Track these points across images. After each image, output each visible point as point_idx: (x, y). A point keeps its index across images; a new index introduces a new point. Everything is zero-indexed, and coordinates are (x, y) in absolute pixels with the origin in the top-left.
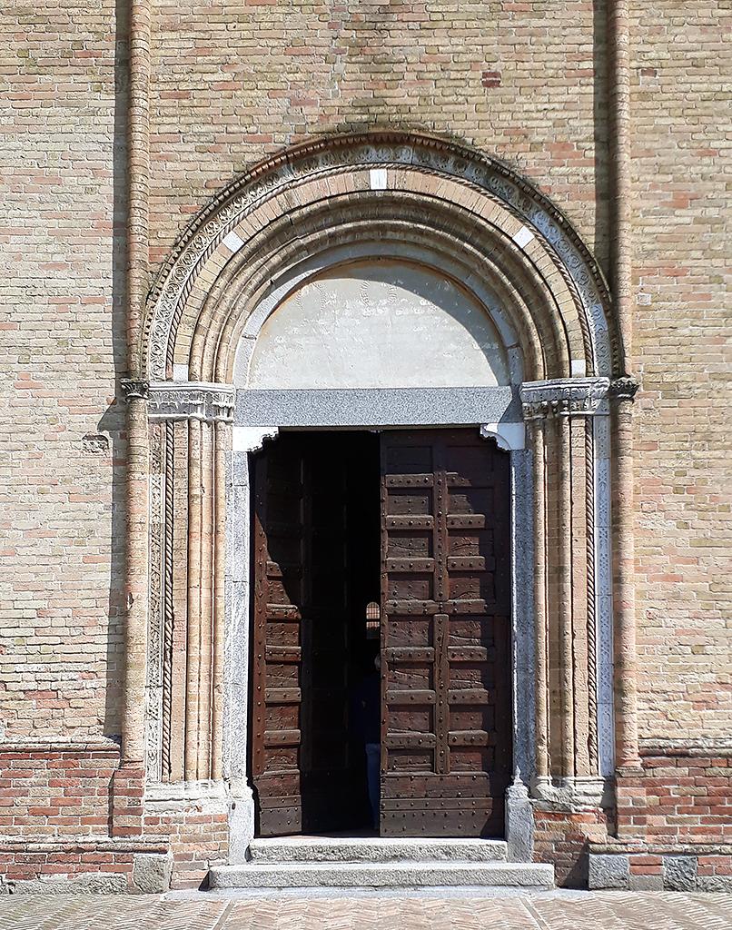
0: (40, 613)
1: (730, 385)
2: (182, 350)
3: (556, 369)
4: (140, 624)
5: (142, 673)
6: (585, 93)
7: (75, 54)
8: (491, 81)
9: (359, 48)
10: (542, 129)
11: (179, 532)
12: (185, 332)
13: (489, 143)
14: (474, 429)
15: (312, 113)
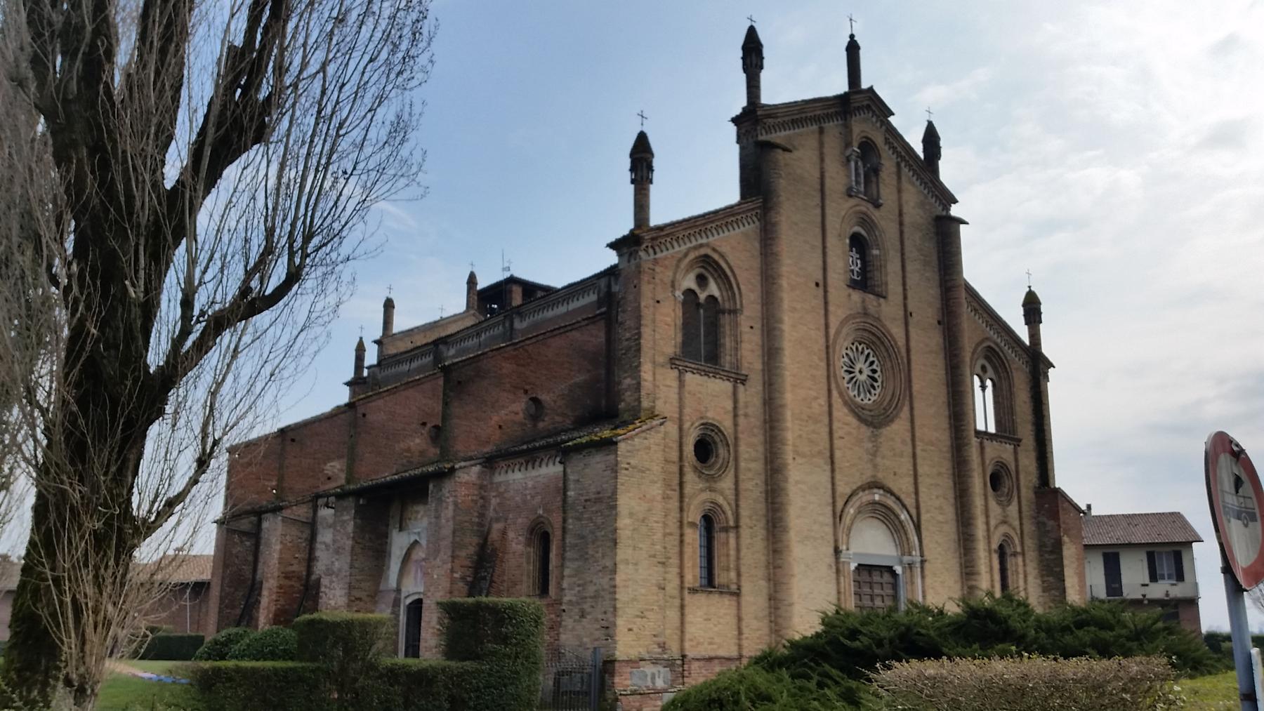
13: (895, 490)
14: (892, 567)
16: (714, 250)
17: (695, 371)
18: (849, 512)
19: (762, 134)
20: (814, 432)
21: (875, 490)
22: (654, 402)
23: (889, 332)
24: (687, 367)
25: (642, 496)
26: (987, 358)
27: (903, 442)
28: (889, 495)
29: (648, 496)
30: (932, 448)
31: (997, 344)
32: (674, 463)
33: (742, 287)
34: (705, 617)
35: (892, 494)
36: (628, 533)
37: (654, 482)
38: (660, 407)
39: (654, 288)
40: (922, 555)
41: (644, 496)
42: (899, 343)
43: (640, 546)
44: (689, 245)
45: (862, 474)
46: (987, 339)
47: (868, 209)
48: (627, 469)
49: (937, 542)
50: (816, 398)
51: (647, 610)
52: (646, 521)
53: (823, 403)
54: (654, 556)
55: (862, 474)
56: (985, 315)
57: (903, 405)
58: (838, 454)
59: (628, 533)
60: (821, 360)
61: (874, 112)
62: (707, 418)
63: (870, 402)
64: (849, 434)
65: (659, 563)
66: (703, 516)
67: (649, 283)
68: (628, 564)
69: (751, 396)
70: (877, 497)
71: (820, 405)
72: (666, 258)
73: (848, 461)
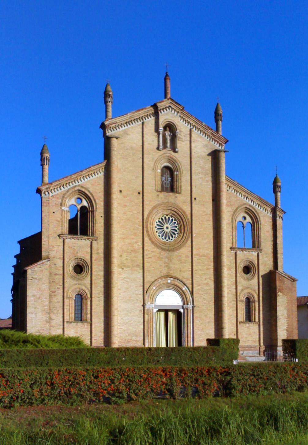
0: (135, 331)
1: (207, 444)
2: (149, 300)
3: (187, 304)
4: (146, 332)
5: (146, 338)
6: (190, 273)
7: (138, 265)
8: (180, 271)
9: (167, 266)
10: (186, 276)
11: (149, 321)
12: (149, 298)
13: (181, 278)
14: (178, 310)
15: (162, 273)
16: (82, 187)
17: (71, 238)
18: (152, 288)
19: (108, 132)
20: (134, 257)
21: (169, 278)
22: (49, 253)
23: (181, 209)
24: (66, 237)
25: (38, 289)
26: (246, 213)
27: (187, 256)
28: (176, 280)
29: (41, 289)
30: (204, 258)
31: (250, 206)
32: (61, 275)
33: (97, 200)
34: (76, 332)
35: (178, 279)
36: (32, 302)
37: (44, 284)
38: (52, 254)
39: (49, 208)
40: (193, 304)
41: (40, 289)
42: (187, 213)
43: (38, 307)
44: (69, 187)
45: (161, 272)
46: (245, 204)
47: (171, 154)
48: (31, 280)
49: (204, 298)
50: (136, 242)
51: (41, 330)
52: (41, 298)
53: (140, 244)
54: (45, 310)
55: (161, 272)
56: (243, 193)
57: (187, 240)
58: (146, 265)
59: (32, 302)
60: (139, 226)
61: (172, 109)
62: (78, 256)
63: (167, 241)
64: (154, 256)
65: (47, 313)
66: (247, 298)
67: (46, 206)
68: (32, 314)
69: (99, 245)
70: (169, 281)
71: (138, 245)
72: (58, 194)
73: (153, 267)
